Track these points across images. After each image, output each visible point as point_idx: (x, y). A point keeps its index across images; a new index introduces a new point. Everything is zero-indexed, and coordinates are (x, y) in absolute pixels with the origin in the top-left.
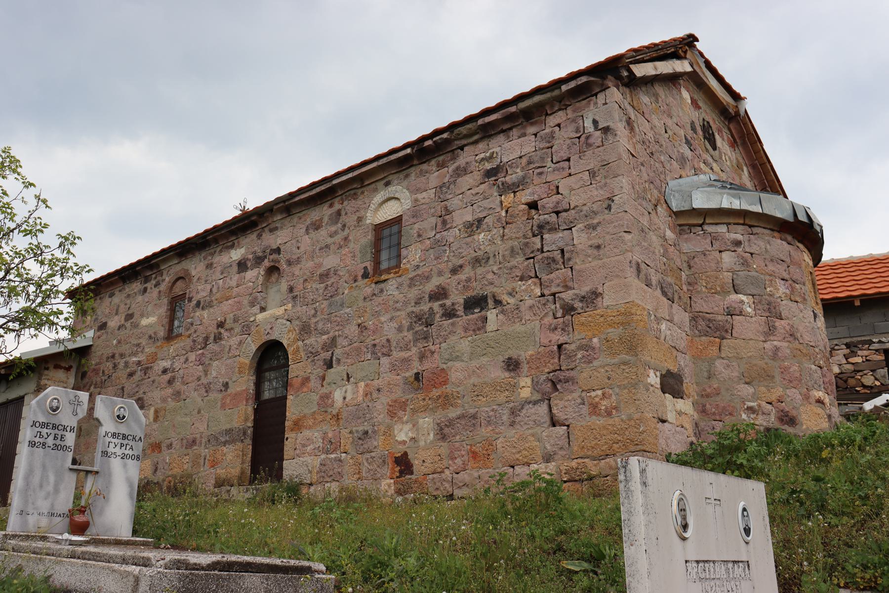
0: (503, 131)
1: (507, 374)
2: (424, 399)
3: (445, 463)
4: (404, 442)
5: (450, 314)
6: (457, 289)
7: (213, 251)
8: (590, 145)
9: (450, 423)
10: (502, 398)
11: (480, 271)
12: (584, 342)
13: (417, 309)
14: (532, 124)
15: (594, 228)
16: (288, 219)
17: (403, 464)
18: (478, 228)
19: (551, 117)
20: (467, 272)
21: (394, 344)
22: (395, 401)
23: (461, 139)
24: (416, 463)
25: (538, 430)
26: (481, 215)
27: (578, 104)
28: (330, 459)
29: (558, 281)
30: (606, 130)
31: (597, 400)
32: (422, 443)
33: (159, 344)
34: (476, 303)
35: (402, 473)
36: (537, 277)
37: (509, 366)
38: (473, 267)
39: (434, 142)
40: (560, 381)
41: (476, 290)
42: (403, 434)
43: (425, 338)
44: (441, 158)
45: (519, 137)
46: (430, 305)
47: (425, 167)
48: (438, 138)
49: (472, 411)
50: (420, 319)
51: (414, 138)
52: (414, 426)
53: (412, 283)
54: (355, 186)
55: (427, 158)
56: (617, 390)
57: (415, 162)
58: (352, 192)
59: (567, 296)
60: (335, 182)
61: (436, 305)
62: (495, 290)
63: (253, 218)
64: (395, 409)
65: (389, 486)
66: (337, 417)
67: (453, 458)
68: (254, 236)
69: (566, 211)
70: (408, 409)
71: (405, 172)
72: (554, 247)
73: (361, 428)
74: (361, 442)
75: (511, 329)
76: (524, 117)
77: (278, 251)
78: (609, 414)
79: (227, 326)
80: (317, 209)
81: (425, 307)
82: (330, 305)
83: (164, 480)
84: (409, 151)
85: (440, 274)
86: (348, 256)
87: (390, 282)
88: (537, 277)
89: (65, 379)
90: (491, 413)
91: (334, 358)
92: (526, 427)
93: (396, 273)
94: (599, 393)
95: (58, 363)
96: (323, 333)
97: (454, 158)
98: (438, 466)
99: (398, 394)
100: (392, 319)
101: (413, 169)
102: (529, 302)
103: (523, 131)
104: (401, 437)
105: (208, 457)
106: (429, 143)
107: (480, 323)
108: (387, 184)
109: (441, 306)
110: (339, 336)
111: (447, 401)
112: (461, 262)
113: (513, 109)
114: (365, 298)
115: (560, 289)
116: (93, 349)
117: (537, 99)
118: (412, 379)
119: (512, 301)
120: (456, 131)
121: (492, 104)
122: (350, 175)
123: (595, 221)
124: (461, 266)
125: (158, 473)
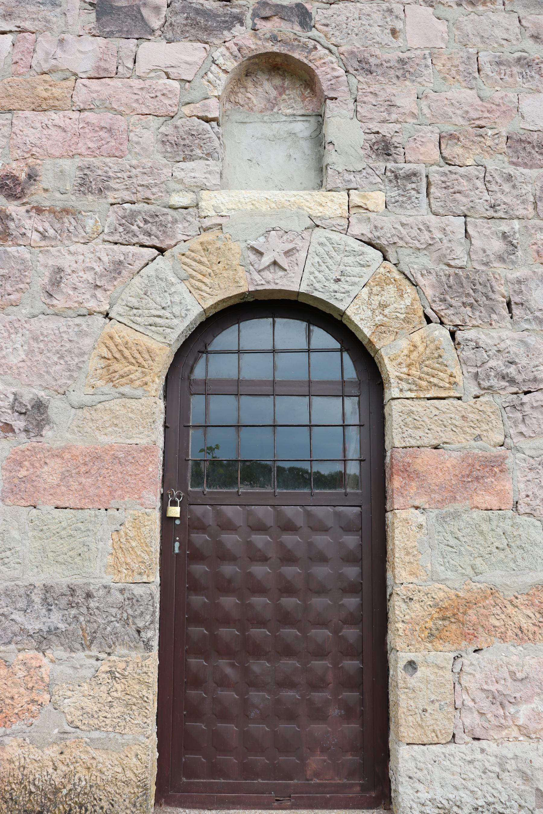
79: (37, 195)
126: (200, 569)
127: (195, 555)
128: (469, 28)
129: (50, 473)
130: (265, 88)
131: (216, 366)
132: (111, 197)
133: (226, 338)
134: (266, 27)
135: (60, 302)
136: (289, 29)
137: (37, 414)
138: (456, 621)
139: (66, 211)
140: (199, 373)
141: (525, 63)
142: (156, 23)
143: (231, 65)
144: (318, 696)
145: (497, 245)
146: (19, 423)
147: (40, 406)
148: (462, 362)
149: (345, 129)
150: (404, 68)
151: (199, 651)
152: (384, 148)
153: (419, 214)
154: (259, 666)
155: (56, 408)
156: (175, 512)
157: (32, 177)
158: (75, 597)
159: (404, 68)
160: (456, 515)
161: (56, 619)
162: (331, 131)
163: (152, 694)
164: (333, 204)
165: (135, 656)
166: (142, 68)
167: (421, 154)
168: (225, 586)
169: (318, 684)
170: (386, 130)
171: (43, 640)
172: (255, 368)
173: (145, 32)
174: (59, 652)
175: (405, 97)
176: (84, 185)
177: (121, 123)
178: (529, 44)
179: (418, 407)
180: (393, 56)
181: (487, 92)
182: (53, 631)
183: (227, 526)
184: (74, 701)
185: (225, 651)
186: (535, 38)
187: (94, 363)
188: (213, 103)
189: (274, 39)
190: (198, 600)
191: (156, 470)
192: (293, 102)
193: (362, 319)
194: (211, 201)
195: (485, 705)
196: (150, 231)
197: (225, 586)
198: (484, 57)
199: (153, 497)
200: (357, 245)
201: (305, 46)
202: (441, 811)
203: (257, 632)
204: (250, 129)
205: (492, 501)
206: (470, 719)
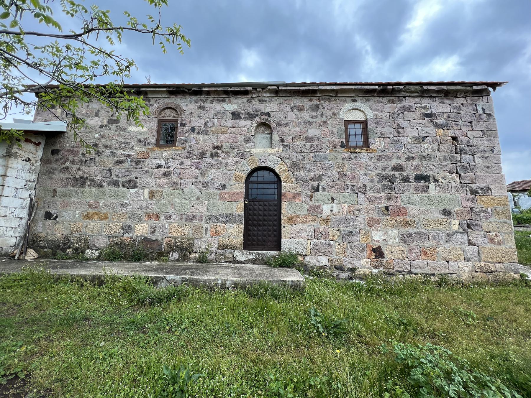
0: (430, 97)
1: (444, 217)
2: (391, 221)
3: (406, 255)
4: (379, 241)
5: (406, 180)
6: (410, 169)
7: (204, 99)
8: (482, 119)
9: (410, 235)
10: (442, 228)
11: (425, 163)
12: (484, 209)
13: (383, 173)
14: (447, 99)
15: (486, 158)
16: (276, 98)
17: (378, 252)
18: (423, 141)
19: (458, 99)
20: (416, 162)
21: (368, 188)
22: (373, 218)
23: (408, 92)
24: (386, 252)
25: (463, 246)
26: (425, 135)
27: (473, 98)
28: (322, 244)
29: (468, 178)
30: (489, 115)
31: (493, 237)
32: (390, 243)
33: (151, 147)
34: (425, 178)
35: (376, 257)
36: (457, 173)
37: (445, 213)
38: (421, 160)
39: (393, 88)
40: (473, 225)
41: (423, 171)
42: (377, 236)
43: (390, 189)
44: (391, 98)
45: (440, 103)
46: (392, 173)
47: (380, 99)
48: (397, 87)
49: (424, 231)
50: (386, 178)
51: (384, 82)
52: (385, 233)
53: (379, 158)
54: (331, 95)
55: (383, 95)
56: (503, 234)
57: (375, 95)
58: (327, 97)
59: (474, 186)
60: (321, 87)
61: (397, 174)
62: (434, 174)
63: (250, 88)
64: (372, 223)
65: (367, 263)
66: (326, 220)
67: (410, 253)
68: (245, 100)
69: (471, 146)
70: (381, 224)
71: (366, 98)
72: (466, 162)
73: (347, 229)
74: (347, 237)
75: (444, 195)
76: (444, 94)
77: (268, 114)
78: (499, 244)
79: (223, 150)
80: (299, 99)
81: (390, 173)
82: (315, 156)
83: (162, 239)
84: (377, 87)
85: (399, 158)
86: (329, 133)
87: (363, 154)
88: (457, 173)
89: (35, 152)
90: (436, 234)
91: (320, 187)
92: (455, 244)
93: (367, 150)
94: (494, 234)
95: (29, 138)
96: (310, 171)
97: (400, 101)
98: (401, 256)
99: (374, 215)
100: (366, 174)
101: (372, 98)
102: (454, 185)
103: (442, 100)
104: (376, 238)
105: (209, 229)
106: (390, 87)
107: (425, 189)
108: (354, 101)
109: (400, 174)
110: (323, 175)
111: (407, 224)
112: (412, 155)
113: (445, 88)
114: (343, 159)
115: (469, 182)
116: (66, 135)
117: (459, 87)
118: (384, 209)
119: (444, 181)
120: (407, 87)
121: (435, 81)
122: (333, 87)
123: (486, 155)
124: (413, 158)
125: (156, 234)
126: (250, 212)
127: (250, 210)
128: (299, 116)
129: (226, 196)
130: (261, 129)
131: (254, 179)
132: (236, 150)
133: (255, 174)
134: (262, 117)
135: (227, 168)
136: (266, 117)
137: (224, 187)
138: (292, 220)
139: (228, 152)
140: (251, 180)
141: (309, 123)
142: (242, 117)
143: (256, 125)
144: (270, 233)
145: (301, 157)
146: (221, 188)
147: (224, 185)
148: (294, 178)
149: (276, 137)
150: (287, 125)
151: (250, 225)
152: (282, 140)
153: (288, 152)
154: (260, 228)
155: (227, 185)
156: (247, 202)
157: (222, 146)
158: (231, 215)
159: (287, 125)
160: (292, 203)
161: (227, 219)
162: (273, 138)
163: (243, 230)
164: (273, 151)
165: (240, 224)
166: (240, 126)
167: (289, 141)
168: (255, 215)
169: (270, 231)
170: (283, 137)
171: (225, 222)
172: (260, 179)
173: (240, 118)
174: (228, 224)
175: (286, 130)
176: (231, 148)
177: (237, 136)
178: (311, 119)
179: (286, 185)
180: (285, 122)
181: (302, 129)
182: (227, 221)
183: (255, 205)
184: (231, 231)
185: (255, 225)
186: (312, 117)
187: (233, 178)
188: (253, 132)
189: (264, 119)
190: (250, 217)
191: (243, 195)
192: (267, 131)
193: (277, 171)
194: (252, 150)
195: (296, 233)
196: (242, 155)
197: (255, 215)
198: (302, 122)
199: (243, 200)
200: (277, 158)
201: (269, 121)
202: (339, 362)
203: (260, 222)
204: (259, 136)
205: (298, 201)
206: (293, 235)
